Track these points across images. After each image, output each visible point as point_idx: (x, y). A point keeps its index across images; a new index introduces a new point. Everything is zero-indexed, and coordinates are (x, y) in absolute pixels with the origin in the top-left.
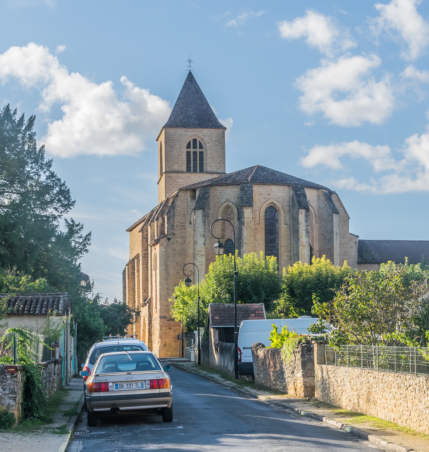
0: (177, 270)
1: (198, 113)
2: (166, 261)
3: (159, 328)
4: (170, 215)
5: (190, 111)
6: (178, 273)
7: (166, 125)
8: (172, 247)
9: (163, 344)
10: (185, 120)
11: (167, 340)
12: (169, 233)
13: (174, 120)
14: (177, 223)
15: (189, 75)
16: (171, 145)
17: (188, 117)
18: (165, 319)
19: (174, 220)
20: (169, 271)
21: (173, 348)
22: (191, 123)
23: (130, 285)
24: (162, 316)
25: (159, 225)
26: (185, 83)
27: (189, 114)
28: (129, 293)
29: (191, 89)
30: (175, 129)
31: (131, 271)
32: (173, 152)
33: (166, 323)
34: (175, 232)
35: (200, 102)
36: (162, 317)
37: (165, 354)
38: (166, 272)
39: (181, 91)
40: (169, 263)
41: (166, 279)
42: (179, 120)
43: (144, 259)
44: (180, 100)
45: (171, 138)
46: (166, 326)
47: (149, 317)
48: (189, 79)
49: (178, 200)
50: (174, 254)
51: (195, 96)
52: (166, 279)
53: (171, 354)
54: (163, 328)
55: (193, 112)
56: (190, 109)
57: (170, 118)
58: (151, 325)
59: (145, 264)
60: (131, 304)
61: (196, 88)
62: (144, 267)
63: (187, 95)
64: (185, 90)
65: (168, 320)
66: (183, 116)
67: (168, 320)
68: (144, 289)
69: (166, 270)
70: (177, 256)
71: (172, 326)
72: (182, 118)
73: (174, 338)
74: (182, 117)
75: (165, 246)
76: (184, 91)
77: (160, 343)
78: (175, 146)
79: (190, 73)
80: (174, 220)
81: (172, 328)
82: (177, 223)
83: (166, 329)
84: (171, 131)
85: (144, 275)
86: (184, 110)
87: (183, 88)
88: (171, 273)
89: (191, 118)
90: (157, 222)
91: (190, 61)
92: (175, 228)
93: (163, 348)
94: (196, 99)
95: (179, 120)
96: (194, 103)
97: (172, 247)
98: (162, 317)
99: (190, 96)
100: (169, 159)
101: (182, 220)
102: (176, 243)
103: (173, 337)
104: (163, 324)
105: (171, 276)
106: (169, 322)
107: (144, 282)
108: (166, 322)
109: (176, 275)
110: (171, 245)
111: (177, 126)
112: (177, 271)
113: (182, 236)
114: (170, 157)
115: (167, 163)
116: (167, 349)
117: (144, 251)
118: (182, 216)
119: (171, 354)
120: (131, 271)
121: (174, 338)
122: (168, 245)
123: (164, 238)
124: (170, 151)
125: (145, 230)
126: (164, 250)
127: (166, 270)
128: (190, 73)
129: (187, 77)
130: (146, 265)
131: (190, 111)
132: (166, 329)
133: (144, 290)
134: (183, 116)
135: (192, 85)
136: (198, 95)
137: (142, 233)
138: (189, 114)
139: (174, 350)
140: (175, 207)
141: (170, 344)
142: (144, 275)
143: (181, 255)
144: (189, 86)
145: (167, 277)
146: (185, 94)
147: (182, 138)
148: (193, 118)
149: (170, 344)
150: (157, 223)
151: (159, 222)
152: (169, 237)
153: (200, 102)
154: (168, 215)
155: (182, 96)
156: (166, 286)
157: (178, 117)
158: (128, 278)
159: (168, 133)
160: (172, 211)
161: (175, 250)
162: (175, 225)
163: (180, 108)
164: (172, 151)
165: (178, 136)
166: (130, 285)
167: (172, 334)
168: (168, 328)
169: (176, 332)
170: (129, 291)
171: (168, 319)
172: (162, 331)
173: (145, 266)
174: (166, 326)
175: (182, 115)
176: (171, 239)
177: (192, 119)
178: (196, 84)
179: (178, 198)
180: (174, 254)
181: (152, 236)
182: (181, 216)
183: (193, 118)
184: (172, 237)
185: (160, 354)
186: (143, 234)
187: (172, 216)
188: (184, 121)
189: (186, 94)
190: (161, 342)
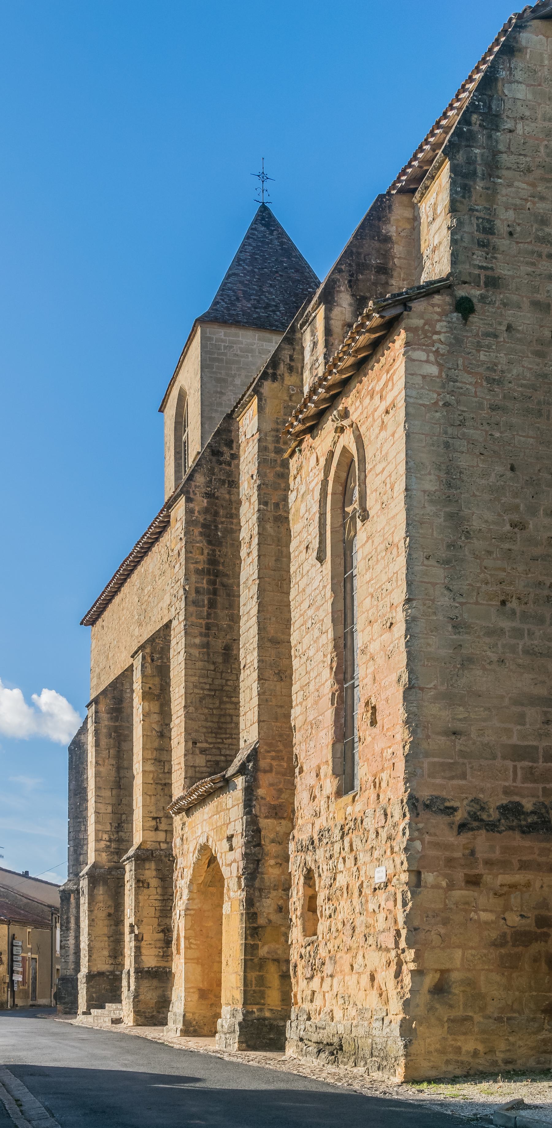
0: (516, 508)
1: (295, 302)
2: (447, 445)
3: (404, 877)
4: (470, 161)
5: (270, 293)
6: (519, 525)
7: (205, 315)
8: (482, 357)
9: (429, 980)
10: (257, 313)
11: (458, 954)
12: (465, 268)
13: (228, 309)
14: (511, 215)
15: (260, 211)
16: (219, 376)
17: (265, 308)
18: (442, 820)
19: (491, 193)
20: (466, 511)
21: (492, 1010)
22: (276, 321)
23: (102, 769)
24: (425, 794)
25: (337, 326)
26: (251, 229)
27: (268, 299)
28: (97, 796)
29: (268, 244)
30: (233, 330)
31: (106, 723)
32: (225, 398)
33: (447, 847)
34: (503, 270)
35: (296, 276)
36: (427, 806)
37: (442, 1052)
38: (450, 516)
39: (243, 245)
40: (464, 461)
41: (447, 562)
42: (242, 311)
43: (192, 609)
44: (240, 265)
45: (219, 354)
46: (450, 862)
47: (247, 844)
48: (263, 219)
49: (519, 75)
50: (494, 408)
51: (282, 262)
52: (447, 562)
53: (480, 1047)
54: (429, 877)
55: (281, 297)
56: (272, 290)
57: (216, 303)
58: (257, 884)
59: (196, 631)
60: (106, 832)
61: (282, 244)
62: (195, 645)
63: (261, 256)
64: (254, 244)
65: (463, 827)
66: (252, 302)
67: (463, 827)
68: (193, 735)
69: (449, 500)
70: (514, 420)
71: (489, 863)
72: (249, 308)
73: (495, 944)
74: (249, 305)
75: (443, 349)
76: (250, 245)
77: (407, 979)
78: (230, 379)
79: (264, 209)
80: (495, 192)
81: (487, 878)
82: (511, 215)
83: (451, 886)
84: (220, 333)
85: (194, 679)
86: (254, 289)
87: (247, 237)
88: (476, 524)
89: (273, 311)
90: (328, 311)
91: (263, 177)
92: (503, 243)
93: (431, 1009)
94: (286, 268)
95: (242, 311)
96: (281, 276)
97: (482, 357)
98: (427, 806)
99: (267, 259)
100: (213, 415)
101: (542, 198)
102: (504, 336)
103: (494, 935)
104: (432, 853)
105: (478, 544)
106: (464, 838)
107: (191, 709)
108: (451, 838)
109: (502, 538)
110: (479, 347)
111: (237, 323)
112: (516, 517)
113: (539, 297)
114: (216, 411)
115: (206, 426)
116: (455, 1013)
117: (193, 578)
118: (543, 179)
119: (480, 1047)
120: (106, 723)
121: (495, 944)
122: (458, 341)
123: (437, 299)
124: (217, 392)
125: (197, 491)
126: (433, 370)
127: (449, 500)
128: (264, 209)
129: (258, 215)
130: (201, 634)
131: (270, 293)
132: (451, 886)
133: (195, 743)
134: (252, 302)
135: (271, 233)
136: (289, 258)
137: (189, 500)
138: (268, 299)
139: (499, 1020)
140: (498, 116)
141: (470, 983)
142: (194, 679)
143: (539, 413)
144: (264, 236)
145: (451, 546)
146: (254, 254)
147: (250, 359)
148: (280, 311)
149: (470, 983)
150: (327, 319)
151: (336, 312)
152: (461, 292)
153: (296, 276)
154: (461, 157)
155: (247, 256)
156: (445, 600)
157: (239, 305)
158: (97, 744)
159: (210, 339)
160: (481, 138)
161: (499, 382)
162: (501, 227)
163: (242, 282)
164: (221, 393)
165: (239, 352)
166: (102, 769)
167: (485, 916)
168: (459, 875)
169: (507, 908)
170: (98, 788)
171: (459, 816)
172: (426, 894)
173: (197, 641)
174: (450, 862)
175: (249, 300)
176: (478, 306)
177: (278, 313)
178: (282, 234)
179: (518, 63)
180: (494, 408)
181: (266, 449)
182: (538, 173)
183: (280, 311)
184: (483, 298)
185: (413, 1049)
186: (191, 505)
187: (479, 169)
188: (255, 316)
189: (257, 254)
190: (417, 974)
